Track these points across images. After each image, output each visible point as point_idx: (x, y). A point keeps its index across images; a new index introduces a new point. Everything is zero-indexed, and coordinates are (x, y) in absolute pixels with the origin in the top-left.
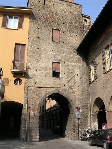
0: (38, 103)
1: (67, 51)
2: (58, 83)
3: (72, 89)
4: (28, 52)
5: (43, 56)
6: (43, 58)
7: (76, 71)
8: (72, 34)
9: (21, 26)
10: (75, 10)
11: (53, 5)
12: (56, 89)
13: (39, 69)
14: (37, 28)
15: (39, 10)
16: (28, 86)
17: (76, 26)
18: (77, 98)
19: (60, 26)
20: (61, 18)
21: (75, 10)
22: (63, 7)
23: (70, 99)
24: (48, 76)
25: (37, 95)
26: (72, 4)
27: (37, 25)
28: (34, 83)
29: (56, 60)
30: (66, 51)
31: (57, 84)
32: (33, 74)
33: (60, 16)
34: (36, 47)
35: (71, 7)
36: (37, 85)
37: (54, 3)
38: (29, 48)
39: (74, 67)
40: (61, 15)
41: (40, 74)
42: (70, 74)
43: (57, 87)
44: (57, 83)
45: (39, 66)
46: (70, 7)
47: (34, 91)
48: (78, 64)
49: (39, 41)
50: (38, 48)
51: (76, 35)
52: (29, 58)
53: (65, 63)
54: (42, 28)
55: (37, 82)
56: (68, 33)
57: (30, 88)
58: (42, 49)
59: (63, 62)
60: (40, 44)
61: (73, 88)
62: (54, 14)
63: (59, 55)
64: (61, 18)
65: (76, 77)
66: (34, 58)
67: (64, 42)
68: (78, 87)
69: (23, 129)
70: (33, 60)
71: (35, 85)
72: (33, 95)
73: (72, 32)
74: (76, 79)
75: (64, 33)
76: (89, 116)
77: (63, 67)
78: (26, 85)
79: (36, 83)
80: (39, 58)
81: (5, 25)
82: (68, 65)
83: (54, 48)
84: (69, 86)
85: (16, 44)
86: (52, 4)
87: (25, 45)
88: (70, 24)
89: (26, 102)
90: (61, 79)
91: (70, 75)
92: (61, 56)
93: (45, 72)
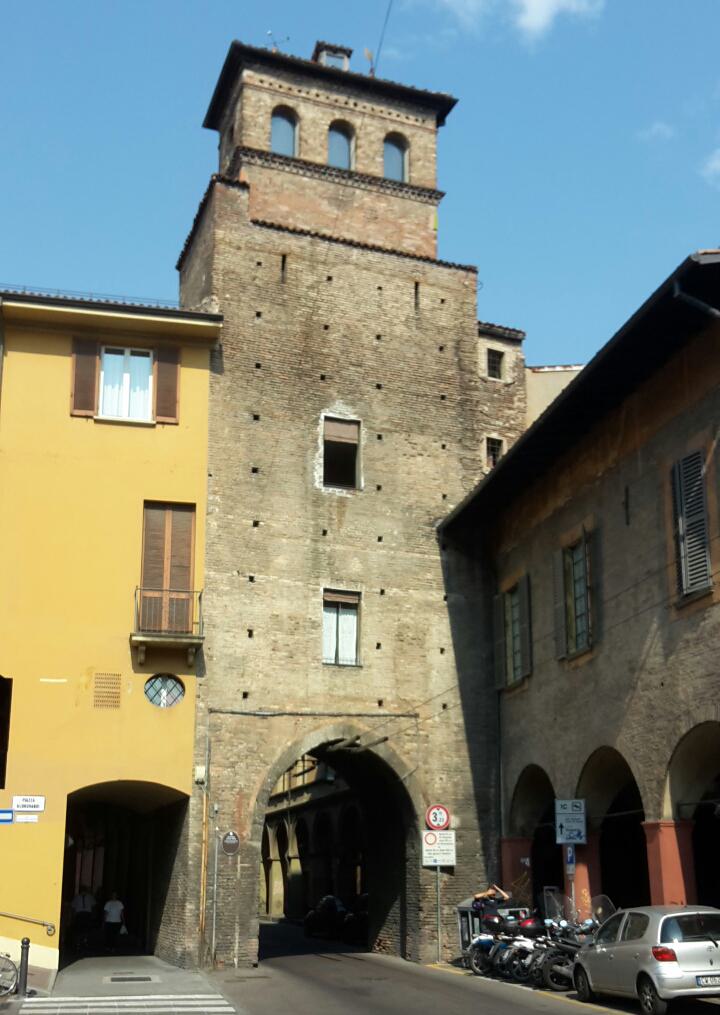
0: (258, 786)
1: (396, 533)
2: (351, 691)
4: (210, 545)
5: (281, 561)
6: (281, 573)
7: (433, 630)
9: (166, 405)
10: (443, 301)
11: (330, 279)
14: (247, 416)
15: (259, 315)
16: (211, 711)
17: (443, 397)
18: (435, 764)
19: (360, 400)
20: (368, 353)
21: (443, 301)
22: (380, 288)
23: (402, 764)
24: (303, 660)
26: (427, 266)
27: (248, 403)
28: (241, 696)
29: (339, 580)
30: (391, 534)
31: (346, 698)
32: (231, 651)
33: (365, 341)
34: (246, 517)
35: (421, 289)
36: (250, 705)
37: (334, 265)
38: (214, 524)
39: (425, 611)
40: (368, 339)
41: (267, 652)
42: (406, 647)
43: (343, 711)
44: (342, 693)
45: (259, 611)
46: (417, 285)
47: (236, 732)
49: (262, 489)
50: (256, 524)
51: (438, 445)
52: (212, 573)
53: (382, 592)
55: (253, 688)
57: (222, 716)
59: (371, 587)
61: (416, 716)
62: (333, 336)
63: (356, 554)
64: (368, 353)
65: (435, 658)
66: (235, 573)
67: (379, 488)
69: (191, 910)
70: (231, 582)
71: (241, 705)
73: (423, 430)
74: (434, 673)
75: (380, 437)
77: (371, 613)
78: (202, 705)
79: (245, 695)
80: (260, 572)
81: (84, 398)
82: (397, 602)
85: (149, 505)
87: (190, 507)
88: (414, 388)
90: (363, 672)
92: (364, 561)
93: (290, 640)
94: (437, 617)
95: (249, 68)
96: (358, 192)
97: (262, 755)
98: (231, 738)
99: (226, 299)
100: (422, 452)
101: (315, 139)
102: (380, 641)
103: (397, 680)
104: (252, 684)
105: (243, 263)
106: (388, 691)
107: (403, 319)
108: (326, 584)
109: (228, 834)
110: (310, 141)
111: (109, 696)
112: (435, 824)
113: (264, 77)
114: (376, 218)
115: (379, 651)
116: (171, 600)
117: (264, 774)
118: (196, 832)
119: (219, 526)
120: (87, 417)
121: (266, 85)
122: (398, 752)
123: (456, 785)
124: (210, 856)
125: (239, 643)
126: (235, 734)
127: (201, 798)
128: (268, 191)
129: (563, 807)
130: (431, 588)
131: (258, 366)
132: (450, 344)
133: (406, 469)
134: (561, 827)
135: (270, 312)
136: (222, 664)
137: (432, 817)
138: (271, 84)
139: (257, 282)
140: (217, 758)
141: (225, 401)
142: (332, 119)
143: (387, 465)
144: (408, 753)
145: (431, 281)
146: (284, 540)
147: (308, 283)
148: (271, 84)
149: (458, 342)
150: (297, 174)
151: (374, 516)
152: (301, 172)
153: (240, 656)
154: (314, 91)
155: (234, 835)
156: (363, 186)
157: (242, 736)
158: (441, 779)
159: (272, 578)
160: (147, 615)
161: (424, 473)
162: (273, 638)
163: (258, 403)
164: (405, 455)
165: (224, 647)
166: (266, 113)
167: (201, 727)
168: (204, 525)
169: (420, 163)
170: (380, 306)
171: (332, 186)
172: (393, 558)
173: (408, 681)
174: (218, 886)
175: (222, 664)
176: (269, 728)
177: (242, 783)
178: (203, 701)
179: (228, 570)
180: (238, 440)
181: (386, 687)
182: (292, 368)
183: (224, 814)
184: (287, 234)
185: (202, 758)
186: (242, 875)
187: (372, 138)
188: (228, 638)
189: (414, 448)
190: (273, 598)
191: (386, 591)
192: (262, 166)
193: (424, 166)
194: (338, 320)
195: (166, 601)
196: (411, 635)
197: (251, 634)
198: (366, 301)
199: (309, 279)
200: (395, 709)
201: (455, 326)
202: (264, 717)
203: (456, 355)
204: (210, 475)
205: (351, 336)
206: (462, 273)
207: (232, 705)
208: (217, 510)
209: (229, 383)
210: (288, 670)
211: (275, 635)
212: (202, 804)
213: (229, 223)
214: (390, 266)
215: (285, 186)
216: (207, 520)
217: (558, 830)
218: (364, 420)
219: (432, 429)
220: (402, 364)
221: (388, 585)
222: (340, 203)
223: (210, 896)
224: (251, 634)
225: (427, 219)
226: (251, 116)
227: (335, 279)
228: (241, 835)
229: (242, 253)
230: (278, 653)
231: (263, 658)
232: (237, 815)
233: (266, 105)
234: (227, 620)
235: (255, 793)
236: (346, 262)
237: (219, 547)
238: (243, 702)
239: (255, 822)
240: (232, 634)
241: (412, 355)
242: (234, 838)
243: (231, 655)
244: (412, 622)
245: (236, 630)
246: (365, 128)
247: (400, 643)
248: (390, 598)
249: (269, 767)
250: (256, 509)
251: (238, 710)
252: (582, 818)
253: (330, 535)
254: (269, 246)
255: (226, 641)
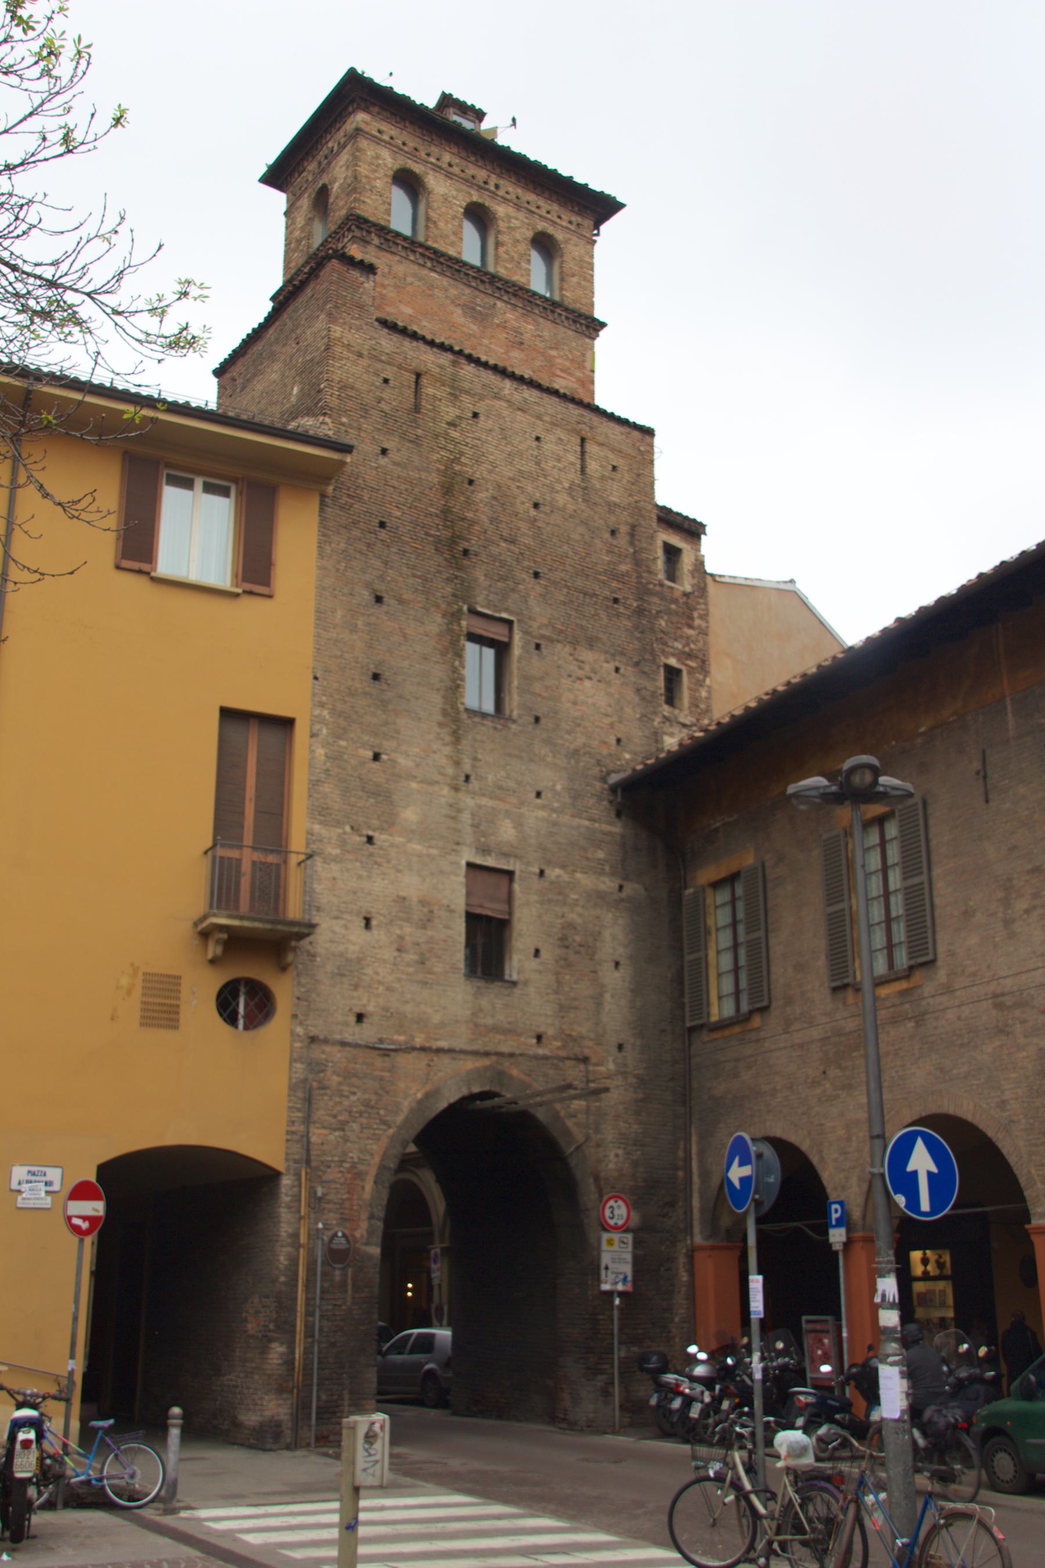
0: (377, 1159)
1: (558, 787)
3: (582, 1067)
4: (314, 784)
5: (410, 815)
7: (607, 934)
8: (588, 656)
9: (255, 566)
10: (614, 468)
11: (475, 415)
12: (486, 1062)
13: (384, 911)
14: (367, 595)
15: (384, 451)
16: (313, 1039)
17: (616, 601)
18: (609, 1133)
19: (513, 590)
20: (523, 526)
21: (614, 468)
23: (567, 1132)
24: (438, 968)
25: (367, 1104)
27: (367, 577)
28: (353, 1019)
29: (485, 851)
31: (495, 1029)
32: (341, 948)
33: (520, 509)
34: (364, 746)
36: (367, 1033)
37: (482, 398)
41: (389, 954)
44: (489, 1021)
45: (380, 888)
48: (621, 887)
49: (384, 704)
50: (376, 757)
51: (611, 666)
52: (317, 827)
53: (542, 873)
54: (401, 601)
55: (371, 1008)
56: (563, 650)
57: (328, 1048)
58: (402, 761)
60: (386, 723)
61: (585, 1060)
64: (523, 526)
66: (348, 829)
68: (620, 1047)
70: (342, 843)
72: (346, 1103)
73: (591, 643)
74: (607, 996)
76: (682, 1260)
78: (300, 1030)
79: (360, 1018)
80: (382, 830)
81: (137, 544)
83: (475, 759)
84: (564, 1047)
85: (228, 714)
86: (468, 403)
87: (287, 723)
88: (579, 583)
89: (297, 1151)
90: (517, 991)
91: (570, 965)
94: (610, 915)
95: (366, 110)
96: (499, 304)
97: (382, 1112)
98: (340, 1083)
99: (343, 424)
100: (592, 675)
101: (447, 222)
102: (540, 946)
103: (561, 1007)
104: (369, 1001)
105: (365, 377)
106: (550, 1021)
107: (567, 485)
108: (468, 855)
109: (335, 1235)
110: (441, 224)
111: (161, 1009)
112: (612, 1222)
113: (384, 126)
114: (522, 343)
115: (537, 960)
116: (254, 863)
117: (385, 1141)
118: (290, 1230)
119: (326, 755)
120: (140, 572)
121: (386, 138)
122: (562, 1114)
123: (635, 1164)
124: (311, 1268)
125: (352, 938)
126: (345, 1078)
127: (298, 1175)
128: (386, 282)
129: (610, 1242)
130: (602, 873)
131: (382, 525)
132: (624, 529)
133: (571, 697)
134: (607, 1268)
135: (399, 450)
136: (329, 968)
137: (608, 1213)
138: (392, 138)
139: (383, 406)
140: (319, 1114)
141: (338, 570)
142: (468, 201)
143: (547, 688)
144: (575, 1116)
145: (601, 439)
146: (414, 785)
147: (449, 418)
148: (392, 138)
149: (633, 527)
150: (423, 266)
151: (531, 760)
152: (429, 264)
153: (354, 956)
154: (447, 158)
155: (344, 1235)
156: (505, 298)
157: (355, 1080)
158: (617, 1155)
159: (399, 840)
160: (223, 887)
161: (594, 704)
162: (398, 932)
163: (382, 578)
164: (570, 676)
165: (332, 941)
166: (386, 175)
167: (298, 1065)
168: (307, 753)
169: (575, 280)
170: (538, 464)
171: (467, 291)
172: (555, 824)
173: (576, 1008)
174: (322, 1316)
175: (329, 968)
176: (391, 1069)
177: (354, 1155)
178: (301, 1023)
179: (339, 824)
180: (354, 629)
181: (546, 1015)
182: (427, 534)
183: (329, 1202)
184: (421, 345)
185: (300, 1114)
186: (353, 1298)
187: (518, 236)
188: (337, 929)
189: (580, 668)
190: (399, 871)
191: (547, 872)
192: (379, 248)
193: (579, 283)
194: (485, 475)
195: (246, 867)
196: (578, 938)
197: (368, 922)
198: (520, 454)
199: (450, 412)
200: (558, 1048)
201: (629, 504)
202: (386, 1053)
203: (632, 543)
204: (316, 678)
205: (501, 499)
206: (636, 434)
207: (341, 1033)
208: (325, 731)
209: (343, 545)
210: (418, 982)
211: (401, 928)
212: (300, 1186)
213: (348, 319)
214: (551, 411)
215: (409, 280)
216: (311, 746)
217: (603, 1272)
218: (519, 621)
219: (604, 644)
220: (565, 547)
221: (549, 863)
222: (470, 310)
223: (309, 1333)
224: (368, 922)
225: (584, 355)
226: (366, 177)
227: (482, 418)
228: (353, 1236)
229: (364, 362)
230: (404, 955)
231: (385, 961)
232: (347, 1205)
233: (386, 165)
234: (335, 900)
235: (373, 1171)
236: (497, 397)
237: (326, 788)
238: (357, 1029)
239: (372, 1217)
240: (342, 922)
241: (577, 537)
242: (343, 1241)
243: (341, 955)
244: (579, 921)
245: (348, 917)
246: (509, 222)
247: (564, 950)
248: (552, 883)
249: (391, 1131)
250: (376, 734)
251: (349, 1038)
252: (629, 1257)
253: (474, 784)
254: (399, 359)
255: (334, 932)
